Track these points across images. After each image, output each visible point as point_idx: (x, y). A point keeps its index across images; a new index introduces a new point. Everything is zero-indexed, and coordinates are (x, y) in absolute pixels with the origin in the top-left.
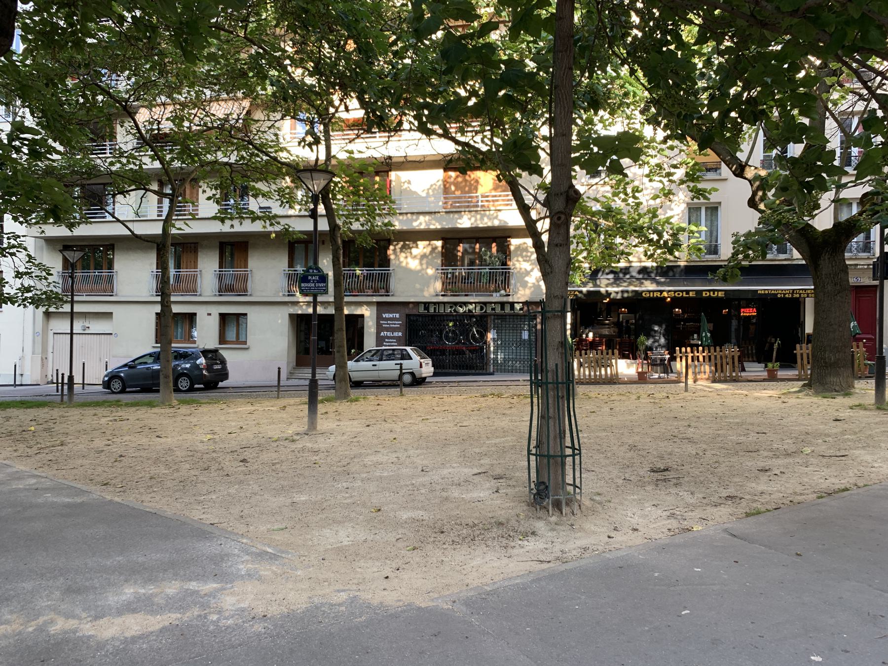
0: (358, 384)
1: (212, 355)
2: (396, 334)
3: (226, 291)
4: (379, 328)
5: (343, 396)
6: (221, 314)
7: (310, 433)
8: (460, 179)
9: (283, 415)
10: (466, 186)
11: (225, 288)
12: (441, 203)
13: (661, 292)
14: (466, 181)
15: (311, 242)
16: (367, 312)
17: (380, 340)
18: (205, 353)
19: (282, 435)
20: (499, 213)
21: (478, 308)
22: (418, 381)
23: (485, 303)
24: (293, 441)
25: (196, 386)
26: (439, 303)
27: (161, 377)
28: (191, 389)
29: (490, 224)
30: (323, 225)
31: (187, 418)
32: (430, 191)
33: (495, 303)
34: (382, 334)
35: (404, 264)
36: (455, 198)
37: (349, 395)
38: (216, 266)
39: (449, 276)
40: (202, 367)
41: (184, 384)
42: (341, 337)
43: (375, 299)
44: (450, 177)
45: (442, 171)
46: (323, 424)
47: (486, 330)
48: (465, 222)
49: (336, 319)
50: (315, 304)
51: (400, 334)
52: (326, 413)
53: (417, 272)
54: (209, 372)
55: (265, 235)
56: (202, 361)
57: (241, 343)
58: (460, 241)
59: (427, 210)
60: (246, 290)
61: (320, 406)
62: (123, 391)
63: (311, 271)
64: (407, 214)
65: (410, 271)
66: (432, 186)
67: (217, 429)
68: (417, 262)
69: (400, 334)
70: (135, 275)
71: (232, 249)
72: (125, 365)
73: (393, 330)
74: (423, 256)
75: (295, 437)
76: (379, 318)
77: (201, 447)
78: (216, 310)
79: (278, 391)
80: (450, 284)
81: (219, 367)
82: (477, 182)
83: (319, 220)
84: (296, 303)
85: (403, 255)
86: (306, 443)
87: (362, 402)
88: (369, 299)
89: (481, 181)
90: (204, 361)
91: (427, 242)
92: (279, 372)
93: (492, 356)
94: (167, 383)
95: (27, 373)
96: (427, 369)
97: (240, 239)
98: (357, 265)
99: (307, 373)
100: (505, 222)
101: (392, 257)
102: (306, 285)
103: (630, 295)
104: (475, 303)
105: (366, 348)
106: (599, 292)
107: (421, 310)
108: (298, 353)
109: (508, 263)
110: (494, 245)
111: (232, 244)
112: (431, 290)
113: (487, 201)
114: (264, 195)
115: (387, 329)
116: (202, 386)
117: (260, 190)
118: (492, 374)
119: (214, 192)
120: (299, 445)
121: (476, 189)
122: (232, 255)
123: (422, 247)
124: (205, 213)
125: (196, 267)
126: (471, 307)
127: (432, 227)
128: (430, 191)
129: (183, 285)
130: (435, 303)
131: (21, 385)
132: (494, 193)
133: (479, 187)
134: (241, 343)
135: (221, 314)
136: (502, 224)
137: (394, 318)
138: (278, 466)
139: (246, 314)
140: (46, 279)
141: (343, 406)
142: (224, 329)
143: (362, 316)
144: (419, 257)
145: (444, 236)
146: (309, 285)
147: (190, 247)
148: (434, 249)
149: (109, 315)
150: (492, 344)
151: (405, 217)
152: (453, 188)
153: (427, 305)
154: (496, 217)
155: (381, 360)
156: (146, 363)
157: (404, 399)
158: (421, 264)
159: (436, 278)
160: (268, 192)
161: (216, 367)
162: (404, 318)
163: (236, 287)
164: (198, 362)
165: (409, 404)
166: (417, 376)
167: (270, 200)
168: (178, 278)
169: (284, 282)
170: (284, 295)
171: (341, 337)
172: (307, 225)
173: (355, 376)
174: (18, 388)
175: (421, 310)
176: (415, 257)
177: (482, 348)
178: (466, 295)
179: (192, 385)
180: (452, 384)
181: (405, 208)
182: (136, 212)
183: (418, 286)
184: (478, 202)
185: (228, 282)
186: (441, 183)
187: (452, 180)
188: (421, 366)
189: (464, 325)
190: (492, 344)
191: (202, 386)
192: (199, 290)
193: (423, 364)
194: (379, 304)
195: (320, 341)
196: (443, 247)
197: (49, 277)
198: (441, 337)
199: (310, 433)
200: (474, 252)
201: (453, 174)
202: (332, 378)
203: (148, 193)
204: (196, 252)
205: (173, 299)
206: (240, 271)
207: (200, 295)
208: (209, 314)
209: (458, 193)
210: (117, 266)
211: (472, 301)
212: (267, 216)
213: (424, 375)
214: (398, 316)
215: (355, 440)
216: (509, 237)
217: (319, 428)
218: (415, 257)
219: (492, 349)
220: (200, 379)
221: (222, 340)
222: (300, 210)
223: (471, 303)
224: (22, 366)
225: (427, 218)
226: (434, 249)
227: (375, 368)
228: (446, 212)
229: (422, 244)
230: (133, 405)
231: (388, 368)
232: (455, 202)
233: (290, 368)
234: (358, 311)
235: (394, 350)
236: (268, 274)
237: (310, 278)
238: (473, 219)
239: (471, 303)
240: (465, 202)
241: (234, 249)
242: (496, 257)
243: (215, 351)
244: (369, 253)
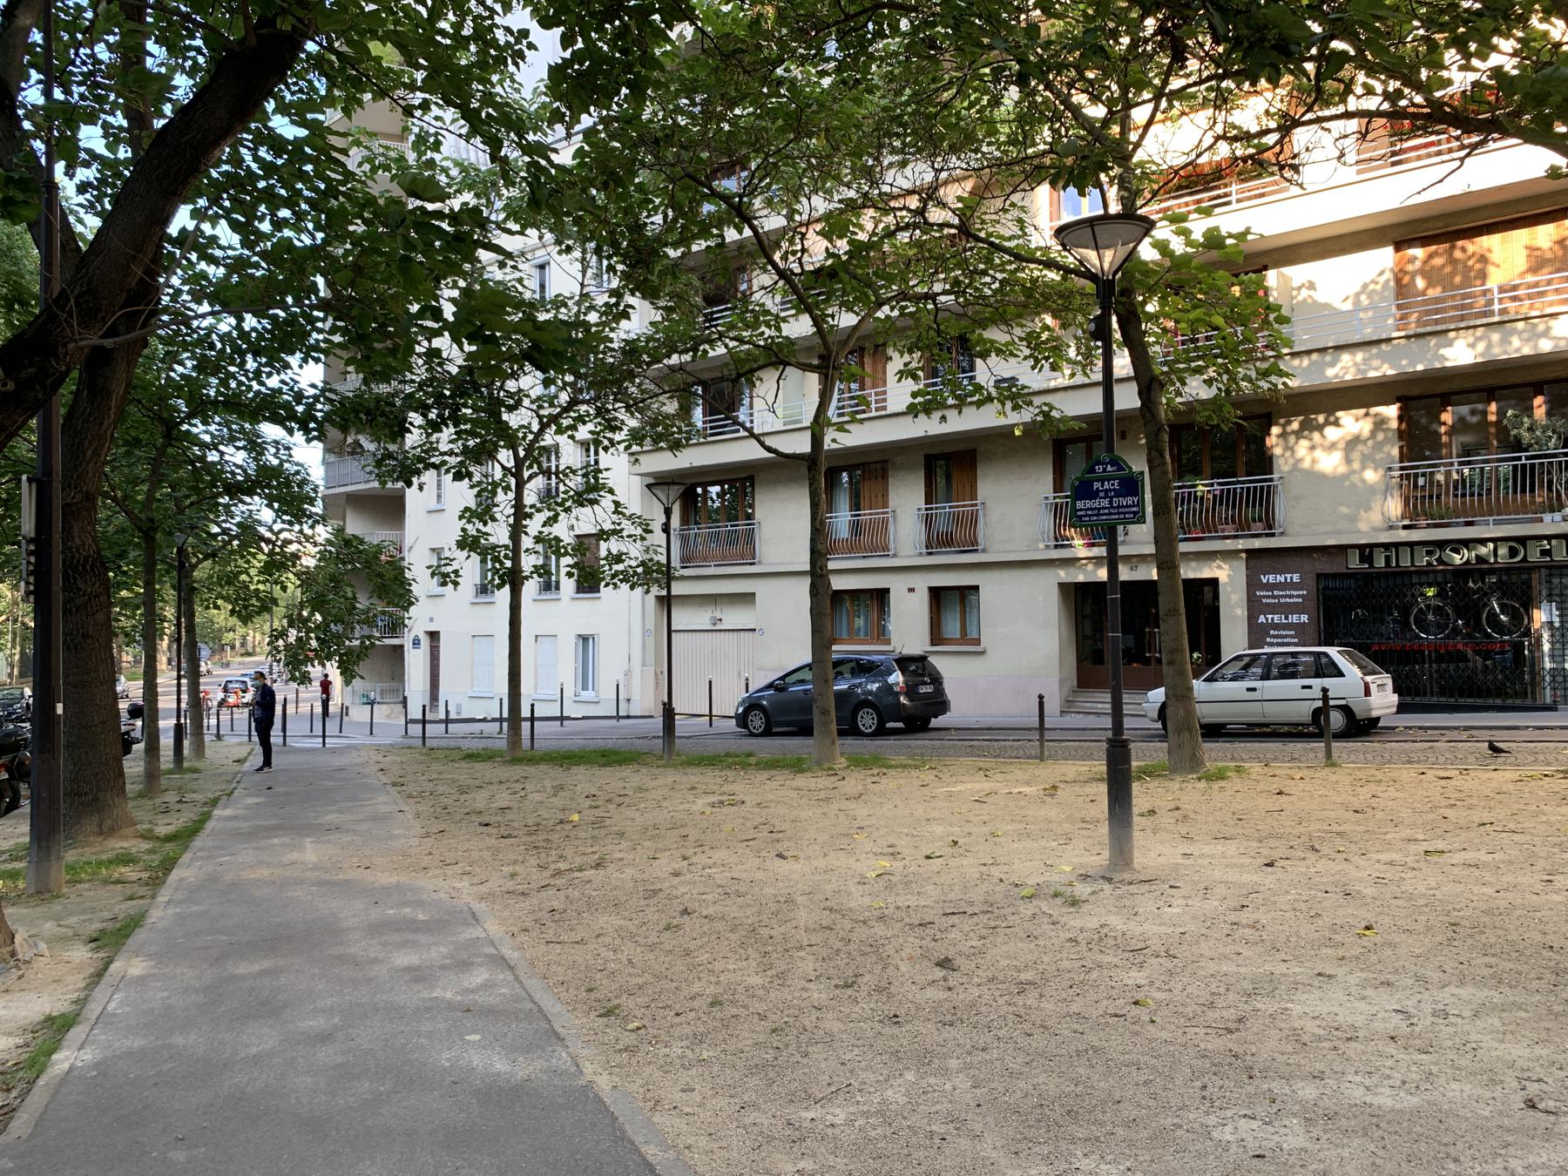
0: (1214, 731)
1: (916, 666)
2: (1294, 619)
3: (939, 545)
4: (1255, 606)
5: (1186, 763)
6: (931, 589)
7: (1117, 877)
8: (1438, 261)
9: (1050, 810)
10: (1453, 274)
11: (937, 540)
12: (1390, 321)
14: (1453, 261)
15: (1100, 438)
16: (1228, 575)
17: (1257, 634)
18: (903, 662)
19: (1047, 877)
20: (1552, 323)
21: (1503, 551)
22: (1361, 727)
23: (1523, 540)
24: (1074, 902)
25: (890, 725)
26: (1397, 545)
27: (816, 712)
28: (881, 732)
29: (1527, 351)
30: (1127, 399)
31: (850, 805)
32: (1363, 297)
33: (1549, 538)
34: (1262, 619)
35: (1306, 464)
36: (1425, 302)
37: (1200, 763)
39: (1421, 481)
40: (897, 689)
41: (867, 721)
42: (1174, 628)
43: (1241, 544)
44: (1413, 260)
45: (1390, 250)
46: (1152, 848)
47: (1528, 603)
48: (1461, 353)
49: (1161, 588)
50: (1112, 561)
51: (1304, 618)
52: (1152, 812)
53: (1340, 480)
54: (911, 700)
55: (1005, 433)
56: (897, 678)
57: (970, 642)
58: (1446, 400)
59: (1357, 338)
60: (975, 542)
61: (1136, 787)
62: (767, 733)
63: (1099, 468)
64: (1309, 352)
65: (1323, 477)
66: (1365, 286)
67: (903, 844)
68: (1338, 456)
69: (1304, 618)
70: (783, 525)
71: (948, 468)
72: (770, 686)
73: (1287, 609)
74: (1353, 442)
75: (1082, 890)
76: (1253, 584)
77: (859, 900)
78: (924, 582)
79: (1042, 740)
80: (1422, 502)
81: (929, 689)
82: (1483, 259)
83: (1118, 390)
84: (1072, 562)
85: (1304, 443)
86: (1105, 912)
87: (1235, 782)
88: (1229, 545)
89: (1493, 257)
90: (901, 679)
91: (1363, 411)
92: (1041, 705)
93: (1548, 665)
94: (826, 724)
95: (636, 697)
96: (1383, 699)
97: (960, 447)
98: (1197, 472)
99: (1101, 701)
101: (1277, 451)
102: (1089, 504)
105: (1227, 654)
107: (1354, 563)
108: (1079, 661)
111: (947, 457)
112: (1375, 518)
113: (1514, 299)
114: (999, 352)
115: (1273, 609)
116: (900, 725)
117: (992, 342)
118: (1552, 708)
119: (907, 358)
120: (1085, 920)
121: (1483, 276)
122: (948, 478)
123: (1352, 423)
124: (894, 407)
125: (885, 505)
126: (1483, 550)
127: (1372, 374)
128: (1363, 297)
129: (865, 539)
130: (1387, 546)
131: (628, 717)
132: (1530, 278)
133: (1491, 269)
134: (970, 642)
135: (931, 589)
137: (1290, 582)
138: (1031, 998)
139: (976, 588)
140: (643, 539)
141: (1187, 791)
142: (939, 618)
143: (1214, 582)
144: (1342, 445)
145: (1404, 392)
146: (1095, 503)
147: (871, 469)
148: (1380, 423)
149: (748, 598)
150: (1546, 636)
151: (1306, 362)
152: (1420, 283)
153: (1366, 551)
154: (1546, 333)
155: (1265, 677)
156: (802, 682)
157: (1339, 776)
158: (1348, 460)
159: (1387, 491)
160: (1007, 344)
161: (923, 689)
162: (1312, 583)
163: (957, 535)
164: (892, 679)
165: (1365, 793)
166: (1360, 714)
167: (1012, 360)
168: (856, 528)
170: (1047, 547)
171: (1174, 628)
172: (1092, 404)
173: (1207, 713)
174: (623, 722)
175: (1354, 563)
176: (1333, 446)
177: (1518, 647)
179: (881, 723)
180: (1455, 735)
181: (1303, 340)
182: (781, 409)
183: (1344, 510)
184: (1490, 302)
185: (941, 526)
186: (1388, 275)
187: (1418, 264)
188: (1367, 693)
189: (1468, 593)
190: (1546, 636)
191: (900, 725)
192: (892, 546)
193: (1373, 688)
194: (1251, 553)
195: (1122, 634)
196: (1400, 418)
197: (647, 536)
198: (1406, 624)
199: (1117, 877)
200: (1484, 423)
201: (1419, 253)
202: (1155, 715)
203: (788, 369)
205: (831, 565)
206: (962, 507)
207: (895, 556)
208: (911, 590)
209: (1434, 293)
210: (761, 512)
211: (1488, 535)
212: (1011, 393)
213: (1375, 714)
214: (1296, 578)
215: (1245, 917)
217: (1138, 859)
218: (1333, 446)
219: (1546, 647)
220: (897, 712)
221: (936, 637)
222: (1073, 375)
223: (1483, 541)
224: (628, 686)
225: (1359, 356)
226: (1380, 423)
227: (1252, 695)
228: (1407, 337)
229: (1346, 417)
230: (772, 765)
231: (1290, 697)
232: (1428, 313)
233: (1066, 690)
234: (1206, 573)
235: (1294, 654)
236: (1015, 507)
237: (1096, 485)
238: (1481, 347)
239: (1483, 541)
240: (1454, 308)
241: (950, 466)
242: (1545, 429)
243: (922, 659)
244: (1227, 449)
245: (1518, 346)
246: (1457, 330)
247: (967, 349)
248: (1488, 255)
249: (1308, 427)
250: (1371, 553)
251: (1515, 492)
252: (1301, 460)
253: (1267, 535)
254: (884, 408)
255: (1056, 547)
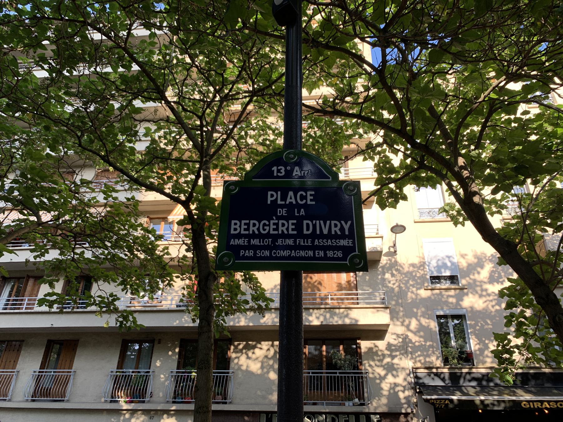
3: (41, 396)
13: (542, 402)
20: (349, 312)
23: (337, 414)
29: (340, 322)
38: (36, 366)
65: (252, 373)
74: (426, 275)
82: (320, 283)
100: (357, 321)
103: (508, 405)
104: (326, 413)
106: (473, 401)
109: (360, 367)
110: (341, 347)
111: (61, 343)
125: (14, 368)
136: (353, 322)
154: (347, 316)
169: (109, 385)
170: (106, 401)
178: (315, 404)
185: (46, 384)
204: (19, 351)
206: (62, 372)
216: (359, 339)
239: (321, 413)
241: (61, 347)
245: (336, 321)
246: (313, 309)
247: (87, 280)
248: (322, 282)
249: (248, 347)
250: (271, 416)
251: (328, 390)
252: (242, 365)
253: (139, 402)
254: (30, 308)
255: (111, 402)
